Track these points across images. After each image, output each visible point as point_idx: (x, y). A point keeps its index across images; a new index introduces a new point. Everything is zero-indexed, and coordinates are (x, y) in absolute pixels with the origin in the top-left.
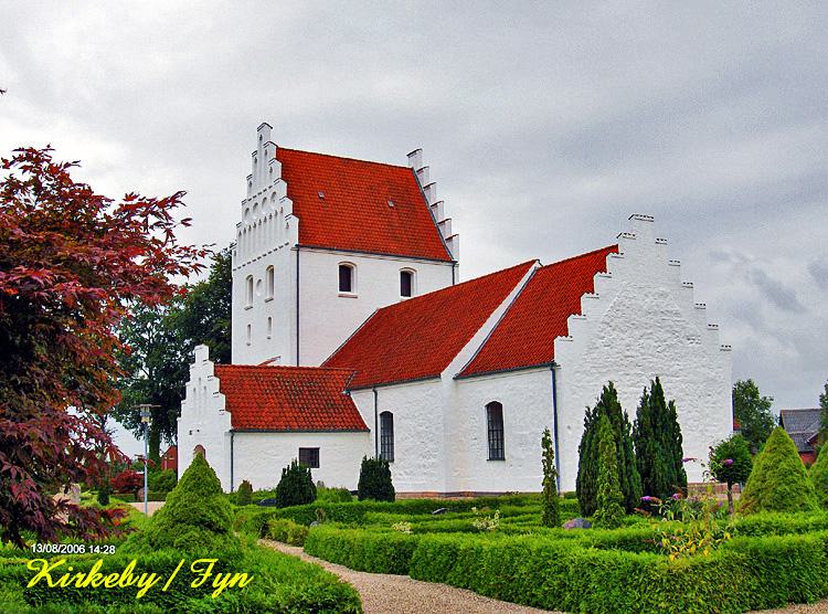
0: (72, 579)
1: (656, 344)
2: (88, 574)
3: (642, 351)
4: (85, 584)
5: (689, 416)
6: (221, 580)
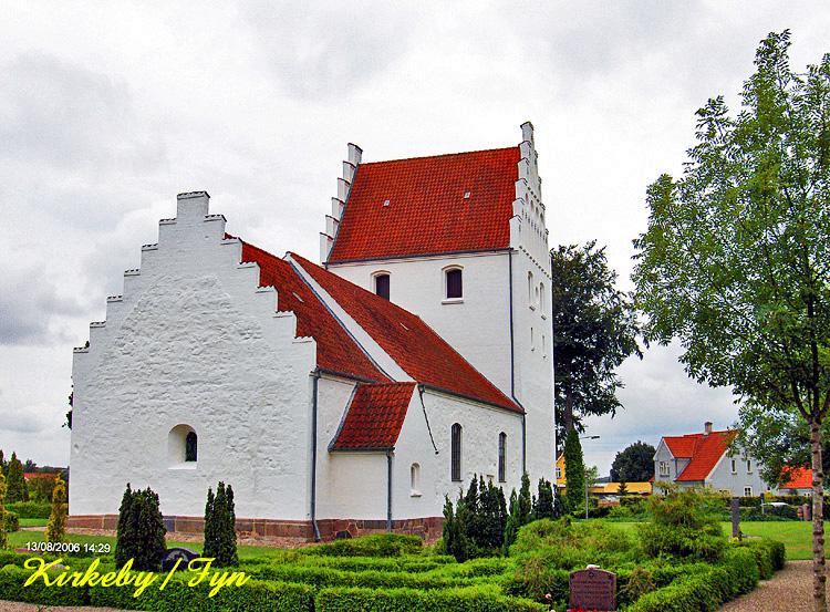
0: (70, 578)
1: (192, 346)
2: (85, 572)
3: (172, 355)
4: (82, 583)
5: (233, 432)
6: (142, 579)
